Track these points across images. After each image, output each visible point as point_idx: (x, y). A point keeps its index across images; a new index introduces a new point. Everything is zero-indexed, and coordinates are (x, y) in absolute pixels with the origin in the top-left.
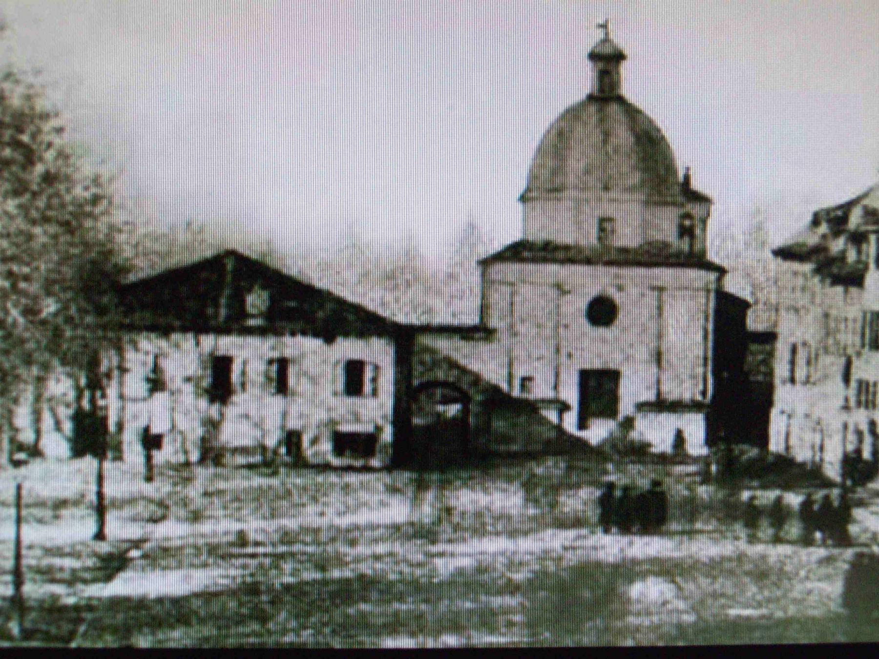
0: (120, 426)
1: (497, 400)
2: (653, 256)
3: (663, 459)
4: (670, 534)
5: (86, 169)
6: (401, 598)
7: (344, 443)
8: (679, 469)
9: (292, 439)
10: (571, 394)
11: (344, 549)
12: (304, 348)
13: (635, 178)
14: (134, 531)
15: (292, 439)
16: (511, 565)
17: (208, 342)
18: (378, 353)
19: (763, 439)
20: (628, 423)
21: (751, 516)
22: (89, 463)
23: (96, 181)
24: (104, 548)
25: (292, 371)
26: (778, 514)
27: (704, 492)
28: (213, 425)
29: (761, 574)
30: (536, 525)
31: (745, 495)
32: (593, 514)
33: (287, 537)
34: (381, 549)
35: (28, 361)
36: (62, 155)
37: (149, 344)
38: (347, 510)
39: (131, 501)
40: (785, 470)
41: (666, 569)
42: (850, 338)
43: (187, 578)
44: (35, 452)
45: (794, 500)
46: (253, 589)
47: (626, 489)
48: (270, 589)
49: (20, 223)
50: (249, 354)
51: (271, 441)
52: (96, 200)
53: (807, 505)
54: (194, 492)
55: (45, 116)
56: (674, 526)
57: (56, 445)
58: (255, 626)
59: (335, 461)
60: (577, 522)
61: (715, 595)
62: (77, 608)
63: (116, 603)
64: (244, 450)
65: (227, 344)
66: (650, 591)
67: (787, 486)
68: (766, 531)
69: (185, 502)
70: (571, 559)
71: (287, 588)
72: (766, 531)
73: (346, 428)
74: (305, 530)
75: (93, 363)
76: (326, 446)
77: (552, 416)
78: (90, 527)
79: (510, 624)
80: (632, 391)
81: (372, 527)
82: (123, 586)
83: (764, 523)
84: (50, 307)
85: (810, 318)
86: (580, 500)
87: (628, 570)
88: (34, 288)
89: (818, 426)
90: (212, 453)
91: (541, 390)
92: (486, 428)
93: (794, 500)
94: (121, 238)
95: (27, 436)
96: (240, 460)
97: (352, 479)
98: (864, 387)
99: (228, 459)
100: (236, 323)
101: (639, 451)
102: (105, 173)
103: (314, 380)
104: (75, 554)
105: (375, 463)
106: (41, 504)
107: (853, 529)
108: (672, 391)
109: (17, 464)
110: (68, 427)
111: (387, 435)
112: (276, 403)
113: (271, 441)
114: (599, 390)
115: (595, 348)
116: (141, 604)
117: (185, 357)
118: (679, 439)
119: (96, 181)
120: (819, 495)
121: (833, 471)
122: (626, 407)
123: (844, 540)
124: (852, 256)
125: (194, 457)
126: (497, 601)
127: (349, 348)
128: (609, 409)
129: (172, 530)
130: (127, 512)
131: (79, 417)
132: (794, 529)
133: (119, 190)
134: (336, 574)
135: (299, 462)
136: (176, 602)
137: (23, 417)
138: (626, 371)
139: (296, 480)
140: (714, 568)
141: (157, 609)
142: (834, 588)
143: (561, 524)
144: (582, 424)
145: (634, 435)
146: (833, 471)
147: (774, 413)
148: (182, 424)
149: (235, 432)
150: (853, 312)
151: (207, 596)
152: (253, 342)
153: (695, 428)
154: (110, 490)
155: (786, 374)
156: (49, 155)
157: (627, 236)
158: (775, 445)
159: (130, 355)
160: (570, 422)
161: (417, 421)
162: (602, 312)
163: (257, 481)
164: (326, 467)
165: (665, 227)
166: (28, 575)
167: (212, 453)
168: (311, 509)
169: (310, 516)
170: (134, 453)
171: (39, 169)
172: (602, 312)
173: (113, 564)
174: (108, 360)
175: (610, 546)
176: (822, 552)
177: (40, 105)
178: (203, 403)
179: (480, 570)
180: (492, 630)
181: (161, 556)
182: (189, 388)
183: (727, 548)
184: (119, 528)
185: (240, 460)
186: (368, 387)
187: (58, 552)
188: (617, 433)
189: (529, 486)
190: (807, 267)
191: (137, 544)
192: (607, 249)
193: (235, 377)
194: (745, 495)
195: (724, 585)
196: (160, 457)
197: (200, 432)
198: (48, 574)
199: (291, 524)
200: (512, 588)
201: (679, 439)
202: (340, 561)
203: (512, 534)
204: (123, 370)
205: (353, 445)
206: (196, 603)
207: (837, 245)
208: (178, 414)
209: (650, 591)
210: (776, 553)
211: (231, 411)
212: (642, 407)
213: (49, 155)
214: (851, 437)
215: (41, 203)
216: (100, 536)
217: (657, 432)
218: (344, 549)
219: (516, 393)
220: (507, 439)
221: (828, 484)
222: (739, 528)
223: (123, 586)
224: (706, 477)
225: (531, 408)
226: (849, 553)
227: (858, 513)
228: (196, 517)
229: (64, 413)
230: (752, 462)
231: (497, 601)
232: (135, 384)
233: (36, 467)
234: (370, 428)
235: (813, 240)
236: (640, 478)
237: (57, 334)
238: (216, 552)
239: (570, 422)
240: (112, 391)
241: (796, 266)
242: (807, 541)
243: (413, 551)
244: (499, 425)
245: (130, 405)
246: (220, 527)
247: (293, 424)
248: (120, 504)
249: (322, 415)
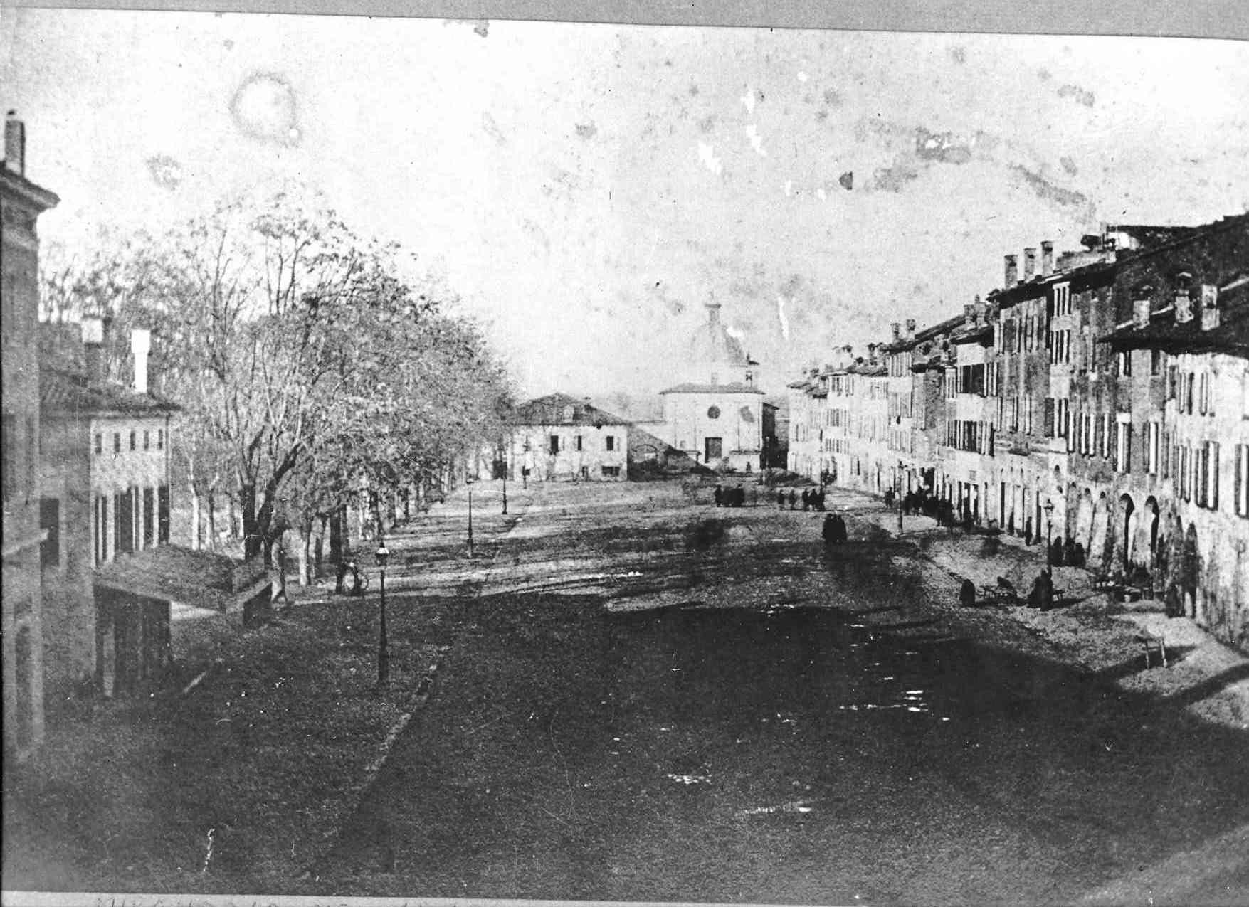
0: (512, 466)
1: (670, 451)
2: (735, 389)
3: (741, 475)
4: (746, 507)
5: (496, 358)
6: (631, 536)
7: (607, 470)
8: (748, 479)
9: (584, 470)
10: (702, 449)
11: (607, 515)
12: (588, 431)
13: (726, 356)
14: (518, 510)
15: (584, 470)
16: (678, 521)
17: (549, 429)
18: (620, 434)
19: (785, 467)
20: (726, 460)
21: (781, 498)
22: (499, 482)
23: (500, 364)
24: (507, 518)
25: (583, 442)
26: (793, 498)
27: (760, 489)
28: (551, 464)
29: (786, 524)
30: (689, 503)
31: (778, 490)
32: (713, 499)
33: (583, 511)
34: (622, 515)
35: (473, 439)
36: (486, 353)
37: (523, 431)
38: (608, 499)
39: (517, 497)
40: (794, 478)
41: (744, 522)
42: (822, 421)
43: (542, 530)
44: (477, 478)
45: (799, 491)
46: (570, 534)
47: (727, 488)
48: (577, 534)
49: (468, 382)
50: (566, 435)
51: (575, 471)
52: (500, 371)
53: (805, 493)
54: (544, 492)
55: (478, 337)
56: (748, 503)
57: (486, 475)
58: (571, 549)
59: (603, 479)
60: (706, 502)
61: (767, 533)
62: (496, 544)
63: (512, 541)
64: (565, 475)
65: (555, 430)
66: (738, 531)
67: (795, 486)
68: (787, 505)
69: (540, 497)
70: (704, 518)
71: (584, 533)
72: (787, 505)
73: (607, 464)
74: (590, 508)
75: (500, 440)
76: (599, 472)
77: (694, 458)
78: (501, 509)
79: (678, 546)
80: (728, 446)
81: (619, 506)
82: (512, 534)
83: (786, 501)
84: (481, 417)
85: (803, 414)
86: (707, 493)
87: (728, 523)
88: (474, 409)
89: (810, 459)
90: (551, 477)
91: (688, 447)
92: (666, 463)
93: (799, 491)
94: (511, 387)
95: (473, 472)
96: (563, 479)
97: (610, 486)
98: (828, 442)
99: (557, 479)
100: (560, 422)
101: (731, 472)
102: (504, 360)
103: (593, 445)
104: (495, 521)
105: (619, 479)
106: (480, 499)
107: (826, 504)
108: (744, 446)
109: (469, 483)
110: (490, 467)
111: (625, 467)
112: (578, 454)
113: (575, 471)
114: (713, 446)
115: (712, 428)
116: (523, 541)
117: (538, 437)
118: (749, 466)
119: (500, 364)
120: (810, 489)
121: (816, 478)
122: (725, 453)
123: (822, 509)
124: (821, 386)
125: (544, 478)
126: (672, 537)
127: (607, 431)
128: (718, 454)
129: (535, 509)
130: (516, 502)
131: (495, 463)
132: (800, 504)
133: (510, 367)
134: (604, 526)
135: (588, 479)
136: (538, 540)
137: (471, 464)
138: (724, 437)
139: (587, 487)
140: (766, 521)
141: (530, 543)
142: (820, 529)
143: (699, 503)
144: (707, 461)
145: (729, 465)
146: (816, 478)
147: (789, 454)
148: (539, 464)
149: (560, 467)
150: (823, 410)
151: (550, 537)
152: (566, 429)
153: (755, 462)
154: (508, 493)
155: (157, 441)
156: (480, 354)
157: (724, 381)
158: (790, 468)
159: (516, 436)
160: (701, 460)
161: (636, 461)
162: (713, 413)
163: (570, 488)
164: (1122, 229)
165: (738, 375)
166: (474, 531)
167: (551, 477)
168: (593, 499)
169: (593, 501)
170: (518, 477)
171: (476, 359)
172: (713, 413)
173: (511, 524)
174: (507, 438)
175: (721, 512)
176: (813, 514)
177: (476, 332)
178: (547, 455)
179: (665, 524)
180: (671, 549)
181: (531, 520)
182: (541, 449)
183: (771, 513)
184: (513, 509)
185: (563, 479)
186: (615, 447)
187: (486, 520)
188: (722, 464)
189: (685, 486)
190: (802, 391)
191: (520, 515)
192: (715, 386)
193: (560, 444)
194: (778, 490)
195: (770, 528)
196: (529, 478)
197: (546, 467)
198: (483, 530)
199: (585, 505)
200: (679, 531)
201: (749, 466)
202: (606, 522)
203: (678, 508)
204: (513, 442)
205: (611, 471)
206: (546, 541)
207: (815, 382)
208: (537, 459)
209: (738, 531)
210: (792, 514)
211: (559, 459)
212: (731, 452)
213: (480, 354)
214: (824, 464)
215: (477, 373)
216: (505, 513)
217: (739, 464)
218: (607, 515)
219: (678, 448)
220: (675, 468)
221: (815, 485)
222: (776, 504)
223: (512, 534)
224: (761, 483)
225: (682, 454)
226: (825, 514)
227: (827, 496)
228: (545, 504)
229: (488, 461)
230: (781, 476)
231: (672, 537)
232: (518, 448)
233: (477, 485)
234: (617, 464)
235: (804, 380)
236: (732, 483)
237: (485, 428)
238: (554, 518)
239: (701, 460)
240: (508, 452)
241: (797, 391)
242: (806, 509)
243: (636, 516)
244: (671, 461)
245: (515, 457)
246: (555, 507)
247: (584, 463)
248: (513, 499)
249: (597, 459)
